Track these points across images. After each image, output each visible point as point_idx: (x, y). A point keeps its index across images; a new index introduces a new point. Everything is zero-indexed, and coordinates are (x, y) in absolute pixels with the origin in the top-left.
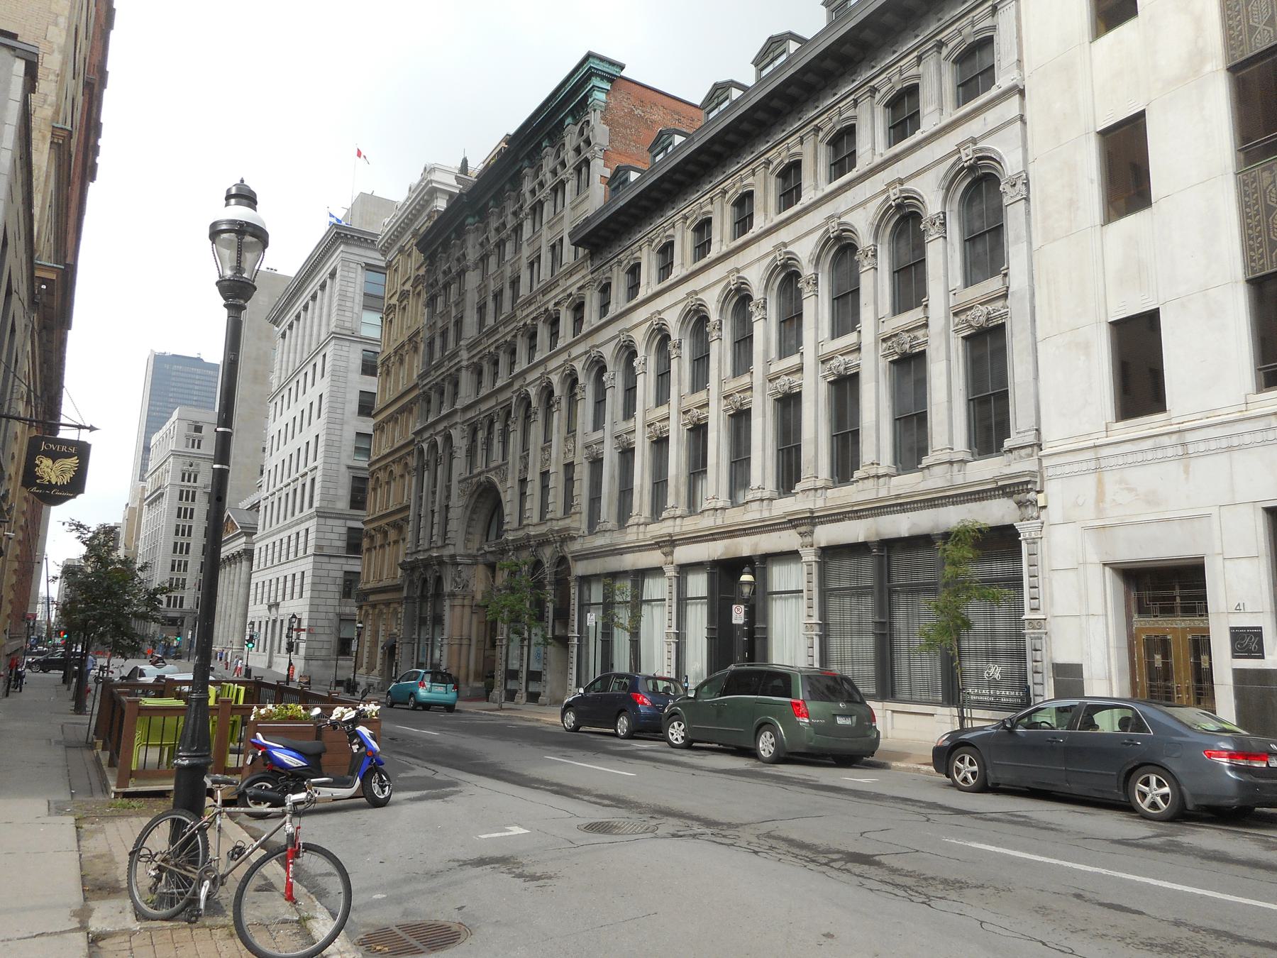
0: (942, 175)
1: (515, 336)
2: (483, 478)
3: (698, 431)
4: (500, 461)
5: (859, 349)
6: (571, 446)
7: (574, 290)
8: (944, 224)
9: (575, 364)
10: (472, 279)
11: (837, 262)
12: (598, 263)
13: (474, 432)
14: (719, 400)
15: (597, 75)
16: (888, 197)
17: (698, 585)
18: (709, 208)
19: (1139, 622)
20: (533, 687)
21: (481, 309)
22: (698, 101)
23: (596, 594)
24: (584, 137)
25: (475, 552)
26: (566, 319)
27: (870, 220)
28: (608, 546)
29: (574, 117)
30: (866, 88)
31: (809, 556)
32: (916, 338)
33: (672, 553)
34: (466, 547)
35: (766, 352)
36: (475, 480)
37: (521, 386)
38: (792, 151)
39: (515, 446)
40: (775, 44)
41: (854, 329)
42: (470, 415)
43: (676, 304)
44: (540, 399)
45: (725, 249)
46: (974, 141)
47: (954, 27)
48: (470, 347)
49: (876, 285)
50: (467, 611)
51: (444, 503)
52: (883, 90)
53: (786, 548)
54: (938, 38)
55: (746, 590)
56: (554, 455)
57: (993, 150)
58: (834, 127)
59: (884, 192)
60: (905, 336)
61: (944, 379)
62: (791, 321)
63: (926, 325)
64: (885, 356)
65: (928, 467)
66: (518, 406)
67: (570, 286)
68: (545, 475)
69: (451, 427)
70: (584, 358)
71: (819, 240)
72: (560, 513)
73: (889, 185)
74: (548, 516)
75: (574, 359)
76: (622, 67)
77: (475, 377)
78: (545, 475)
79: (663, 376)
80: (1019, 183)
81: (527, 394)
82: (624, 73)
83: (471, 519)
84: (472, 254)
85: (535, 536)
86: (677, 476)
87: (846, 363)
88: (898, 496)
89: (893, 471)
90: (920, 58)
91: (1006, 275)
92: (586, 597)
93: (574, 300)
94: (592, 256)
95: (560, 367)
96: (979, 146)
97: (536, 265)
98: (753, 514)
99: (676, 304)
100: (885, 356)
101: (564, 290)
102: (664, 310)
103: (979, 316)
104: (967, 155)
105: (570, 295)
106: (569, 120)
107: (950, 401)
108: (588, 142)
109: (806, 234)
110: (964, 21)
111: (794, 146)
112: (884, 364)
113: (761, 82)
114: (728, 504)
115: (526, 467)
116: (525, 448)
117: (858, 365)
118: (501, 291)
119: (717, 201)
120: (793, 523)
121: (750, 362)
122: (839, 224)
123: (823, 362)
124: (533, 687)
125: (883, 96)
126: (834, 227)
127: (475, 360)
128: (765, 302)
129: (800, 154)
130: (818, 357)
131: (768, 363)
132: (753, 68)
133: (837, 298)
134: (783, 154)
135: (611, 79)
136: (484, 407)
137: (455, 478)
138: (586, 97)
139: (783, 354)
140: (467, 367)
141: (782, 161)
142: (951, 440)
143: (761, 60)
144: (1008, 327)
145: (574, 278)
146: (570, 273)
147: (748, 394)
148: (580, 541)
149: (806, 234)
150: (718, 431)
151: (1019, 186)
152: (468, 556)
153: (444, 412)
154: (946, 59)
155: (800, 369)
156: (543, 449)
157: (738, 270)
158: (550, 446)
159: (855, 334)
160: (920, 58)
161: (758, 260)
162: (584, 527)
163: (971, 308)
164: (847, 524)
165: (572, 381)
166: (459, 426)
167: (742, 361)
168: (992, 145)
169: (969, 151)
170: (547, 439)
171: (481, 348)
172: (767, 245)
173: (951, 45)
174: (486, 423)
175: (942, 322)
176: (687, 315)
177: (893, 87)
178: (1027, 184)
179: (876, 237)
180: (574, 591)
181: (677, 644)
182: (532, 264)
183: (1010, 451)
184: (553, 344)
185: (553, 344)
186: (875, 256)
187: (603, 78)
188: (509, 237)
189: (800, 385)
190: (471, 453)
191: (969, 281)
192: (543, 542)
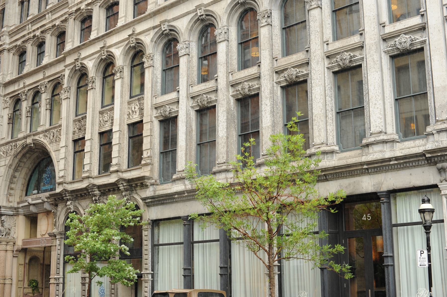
1: (66, 20)
2: (29, 141)
3: (169, 122)
4: (47, 126)
11: (242, 18)
25: (16, 205)
26: (31, 50)
34: (8, 201)
36: (19, 143)
37: (77, 60)
44: (97, 70)
50: (10, 254)
59: (127, 39)
60: (205, 96)
65: (367, 145)
66: (71, 77)
70: (152, 33)
77: (17, 58)
79: (248, 42)
83: (13, 177)
86: (274, 125)
87: (351, 57)
92: (156, 239)
96: (207, 8)
97: (26, 3)
103: (404, 41)
104: (165, 27)
115: (82, 129)
123: (384, 40)
127: (19, 43)
130: (228, 82)
133: (241, 43)
136: (28, 81)
139: (164, 92)
144: (309, 81)
148: (151, 188)
152: (11, 208)
155: (423, 28)
159: (213, 82)
163: (399, 36)
165: (137, 53)
171: (25, 32)
174: (50, 87)
180: (146, 234)
181: (63, 278)
184: (39, 61)
185: (39, 61)
191: (336, 38)
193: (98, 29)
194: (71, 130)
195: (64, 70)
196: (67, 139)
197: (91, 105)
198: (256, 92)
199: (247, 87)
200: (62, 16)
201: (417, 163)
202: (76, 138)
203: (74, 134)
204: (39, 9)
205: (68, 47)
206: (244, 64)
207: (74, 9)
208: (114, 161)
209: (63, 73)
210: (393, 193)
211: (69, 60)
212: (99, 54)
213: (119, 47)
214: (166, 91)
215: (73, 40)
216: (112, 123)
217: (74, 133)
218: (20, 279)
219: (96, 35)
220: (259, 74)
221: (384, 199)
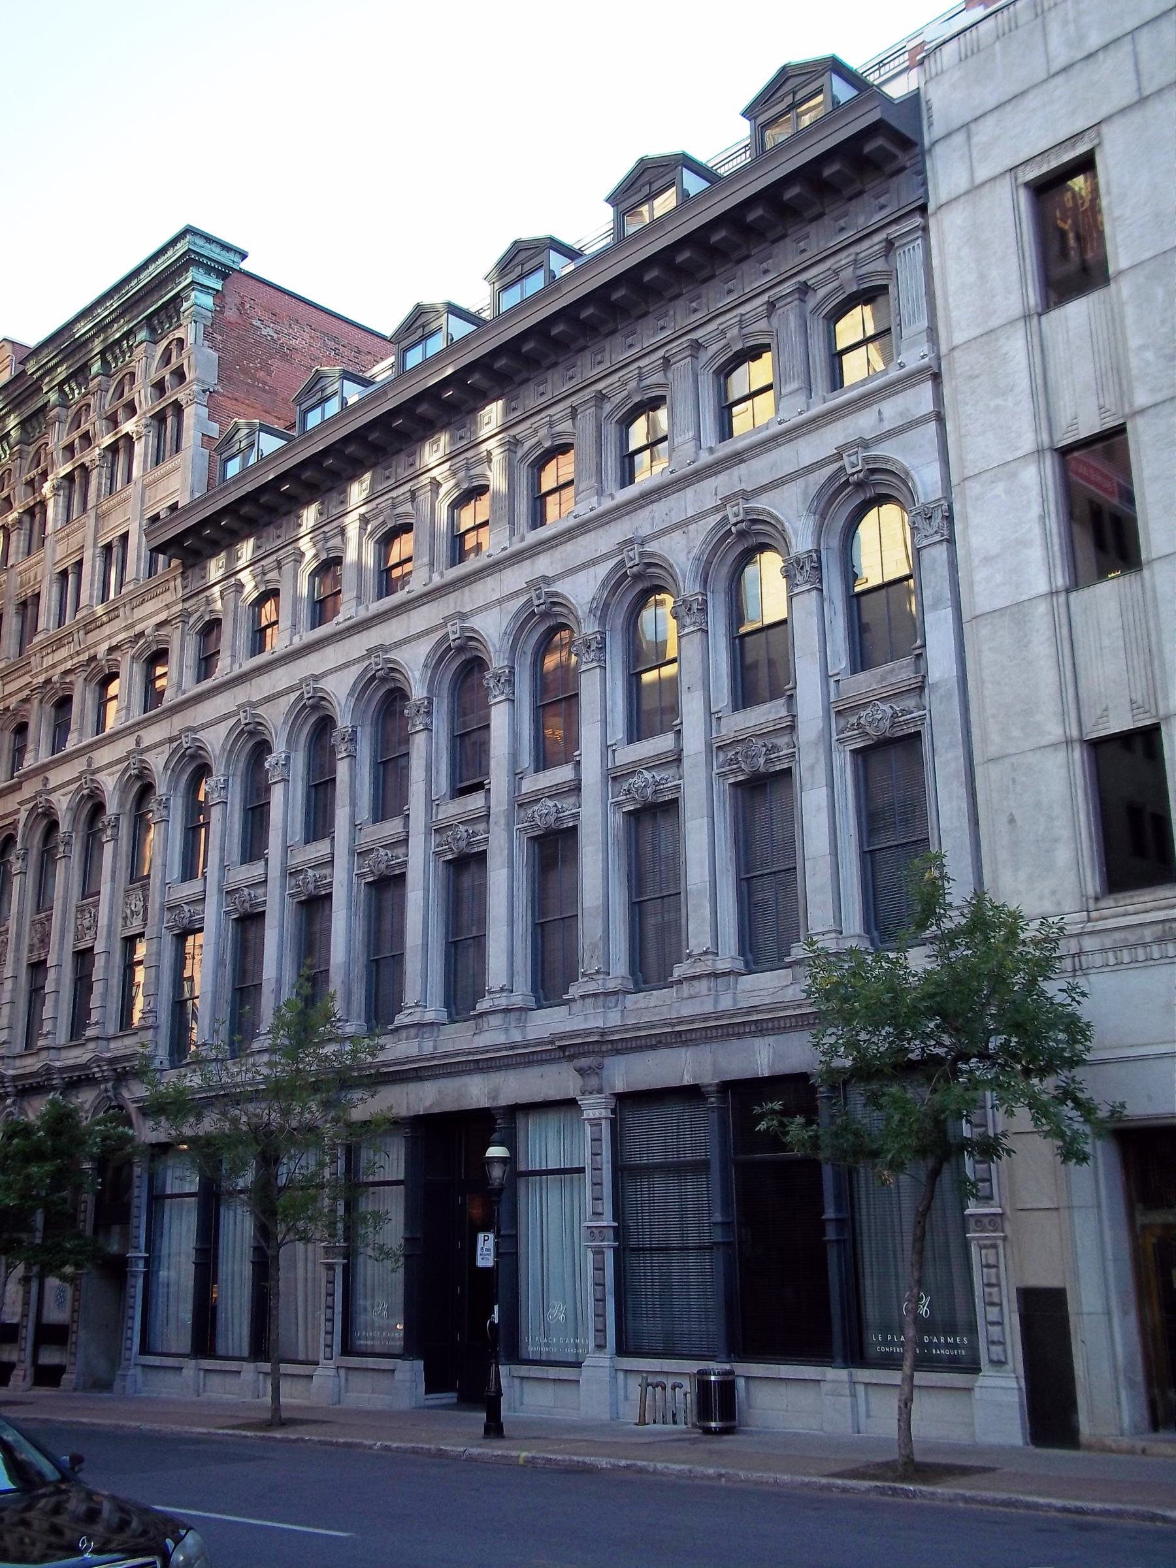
0: (813, 491)
5: (679, 760)
6: (136, 904)
7: (148, 625)
8: (819, 568)
9: (53, 798)
14: (427, 834)
15: (199, 264)
16: (726, 518)
17: (391, 1162)
18: (566, 426)
19: (1140, 1220)
20: (50, 1357)
22: (388, 332)
23: (183, 1180)
24: (80, 431)
27: (695, 552)
28: (706, 1017)
29: (153, 330)
31: (596, 1109)
32: (775, 748)
33: (597, 1070)
35: (514, 757)
37: (38, 794)
39: (22, 902)
40: (649, 177)
41: (671, 728)
43: (346, 665)
45: (363, 614)
46: (865, 444)
47: (735, 312)
52: (714, 348)
53: (553, 1094)
54: (600, 386)
55: (497, 1172)
56: (103, 920)
57: (895, 461)
58: (629, 397)
59: (717, 509)
60: (462, 828)
61: (824, 818)
63: (792, 728)
64: (722, 775)
67: (142, 620)
68: (84, 957)
71: (516, 615)
72: (62, 1038)
73: (726, 500)
74: (41, 1043)
75: (148, 749)
76: (244, 256)
78: (84, 957)
79: (320, 792)
80: (938, 515)
82: (245, 265)
85: (61, 1070)
86: (348, 964)
87: (657, 783)
88: (753, 1009)
89: (739, 965)
90: (772, 305)
91: (919, 656)
95: (119, 761)
98: (492, 1036)
99: (346, 665)
100: (722, 775)
101: (127, 628)
102: (324, 675)
103: (880, 719)
105: (142, 634)
106: (142, 335)
107: (835, 852)
108: (180, 375)
109: (584, 566)
110: (844, 258)
111: (562, 420)
112: (722, 788)
113: (760, 151)
114: (443, 1016)
115: (44, 941)
116: (42, 900)
117: (678, 787)
119: (682, 366)
120: (563, 1051)
121: (403, 797)
122: (641, 554)
124: (50, 1357)
125: (713, 357)
126: (633, 558)
128: (512, 673)
131: (516, 776)
132: (609, 212)
134: (543, 432)
135: (224, 273)
138: (177, 299)
141: (539, 443)
142: (838, 918)
143: (766, 108)
145: (149, 607)
146: (142, 598)
147: (481, 827)
149: (584, 566)
150: (426, 890)
151: (937, 521)
154: (814, 311)
156: (80, 910)
157: (463, 616)
159: (671, 736)
160: (772, 305)
161: (500, 602)
162: (163, 1053)
164: (665, 1054)
167: (388, 798)
168: (476, 622)
169: (310, 688)
170: (89, 890)
172: (358, 645)
173: (821, 293)
175: (819, 724)
176: (367, 682)
177: (728, 345)
178: (949, 518)
179: (705, 582)
183: (679, 982)
184: (58, 741)
185: (58, 741)
186: (703, 610)
187: (209, 270)
189: (576, 816)
192: (79, 1079)
193: (81, 731)
194: (26, 941)
195: (17, 812)
196: (17, 960)
197: (61, 893)
198: (786, 766)
199: (311, 879)
200: (21, 690)
201: (776, 1023)
202: (35, 959)
203: (31, 951)
204: (61, 623)
205: (29, 762)
206: (380, 813)
207: (41, 679)
208: (95, 1016)
209: (16, 817)
210: (517, 1110)
211: (29, 789)
212: (78, 784)
213: (113, 774)
214: (644, 727)
215: (176, 678)
216: (145, 919)
217: (31, 948)
218: (598, 1297)
219: (32, 761)
220: (789, 718)
221: (500, 1123)
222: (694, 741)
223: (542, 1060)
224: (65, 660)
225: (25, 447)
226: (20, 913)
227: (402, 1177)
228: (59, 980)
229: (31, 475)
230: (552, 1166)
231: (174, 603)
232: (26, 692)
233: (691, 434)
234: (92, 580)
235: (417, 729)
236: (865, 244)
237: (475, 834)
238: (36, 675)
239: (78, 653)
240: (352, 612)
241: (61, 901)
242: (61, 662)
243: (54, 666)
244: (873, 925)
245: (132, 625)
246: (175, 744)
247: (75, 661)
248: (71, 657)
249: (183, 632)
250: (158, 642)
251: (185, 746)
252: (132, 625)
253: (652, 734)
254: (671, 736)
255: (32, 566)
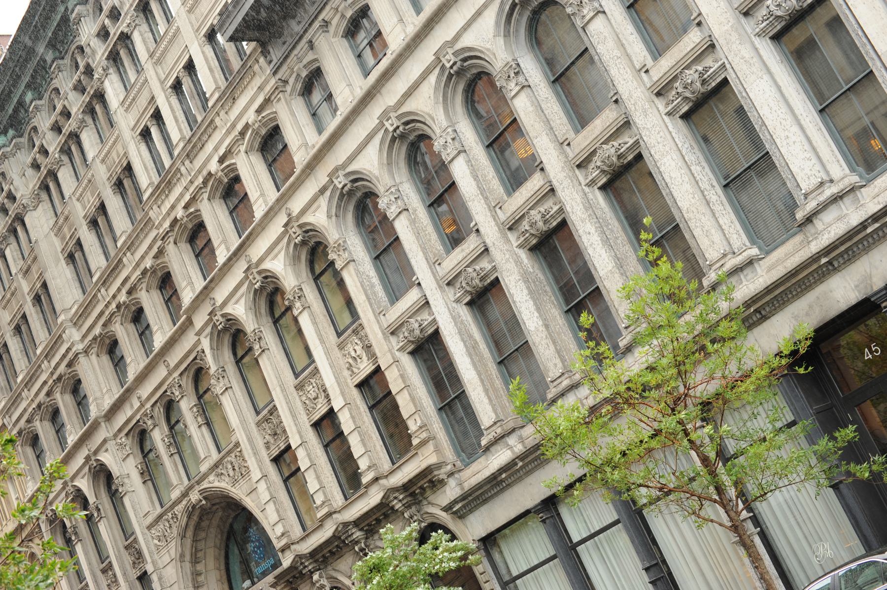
1: (161, 252)
2: (194, 497)
7: (251, 116)
10: (39, 221)
12: (276, 54)
13: (141, 436)
18: (310, 56)
21: (74, 254)
30: (317, 24)
38: (305, 62)
42: (120, 419)
48: (76, 322)
49: (471, 171)
51: (134, 574)
54: (321, 18)
60: (470, 270)
62: (386, 248)
66: (216, 348)
68: (327, 425)
69: (96, 452)
81: (79, 490)
83: (196, 574)
84: (24, 184)
91: (699, 24)
93: (256, 133)
94: (264, 47)
105: (247, 126)
106: (29, 96)
118: (102, 208)
127: (97, 330)
129: (316, 60)
130: (500, 225)
137: (138, 527)
139: (394, 296)
140: (86, 352)
146: (131, 246)
153: (71, 439)
158: (136, 540)
159: (473, 236)
163: (594, 152)
165: (314, 252)
166: (111, 445)
169: (450, 56)
174: (187, 383)
182: (146, 134)
188: (82, 124)
190: (150, 472)
194: (260, 443)
195: (198, 342)
196: (260, 462)
198: (559, 219)
200: (150, 247)
203: (268, 448)
206: (514, 179)
208: (363, 464)
209: (199, 348)
211: (200, 320)
213: (276, 256)
214: (397, 294)
216: (327, 396)
220: (548, 184)
222: (490, 231)
223: (536, 467)
224: (182, 195)
225: (61, 62)
226: (243, 421)
227: (553, 553)
228: (311, 456)
229: (76, 77)
230: (536, 562)
231: (266, 82)
232: (159, 243)
233: (395, 20)
234: (175, 118)
235: (588, 18)
236: (299, 48)
237: (706, 69)
238: (160, 224)
239: (191, 182)
240: (161, 339)
241: (278, 389)
242: (178, 200)
243: (173, 207)
244: (855, 164)
245: (233, 126)
246: (328, 193)
247: (191, 190)
248: (186, 189)
249: (286, 99)
250: (264, 125)
251: (340, 186)
252: (233, 126)
253: (403, 294)
254: (473, 236)
255: (111, 147)
